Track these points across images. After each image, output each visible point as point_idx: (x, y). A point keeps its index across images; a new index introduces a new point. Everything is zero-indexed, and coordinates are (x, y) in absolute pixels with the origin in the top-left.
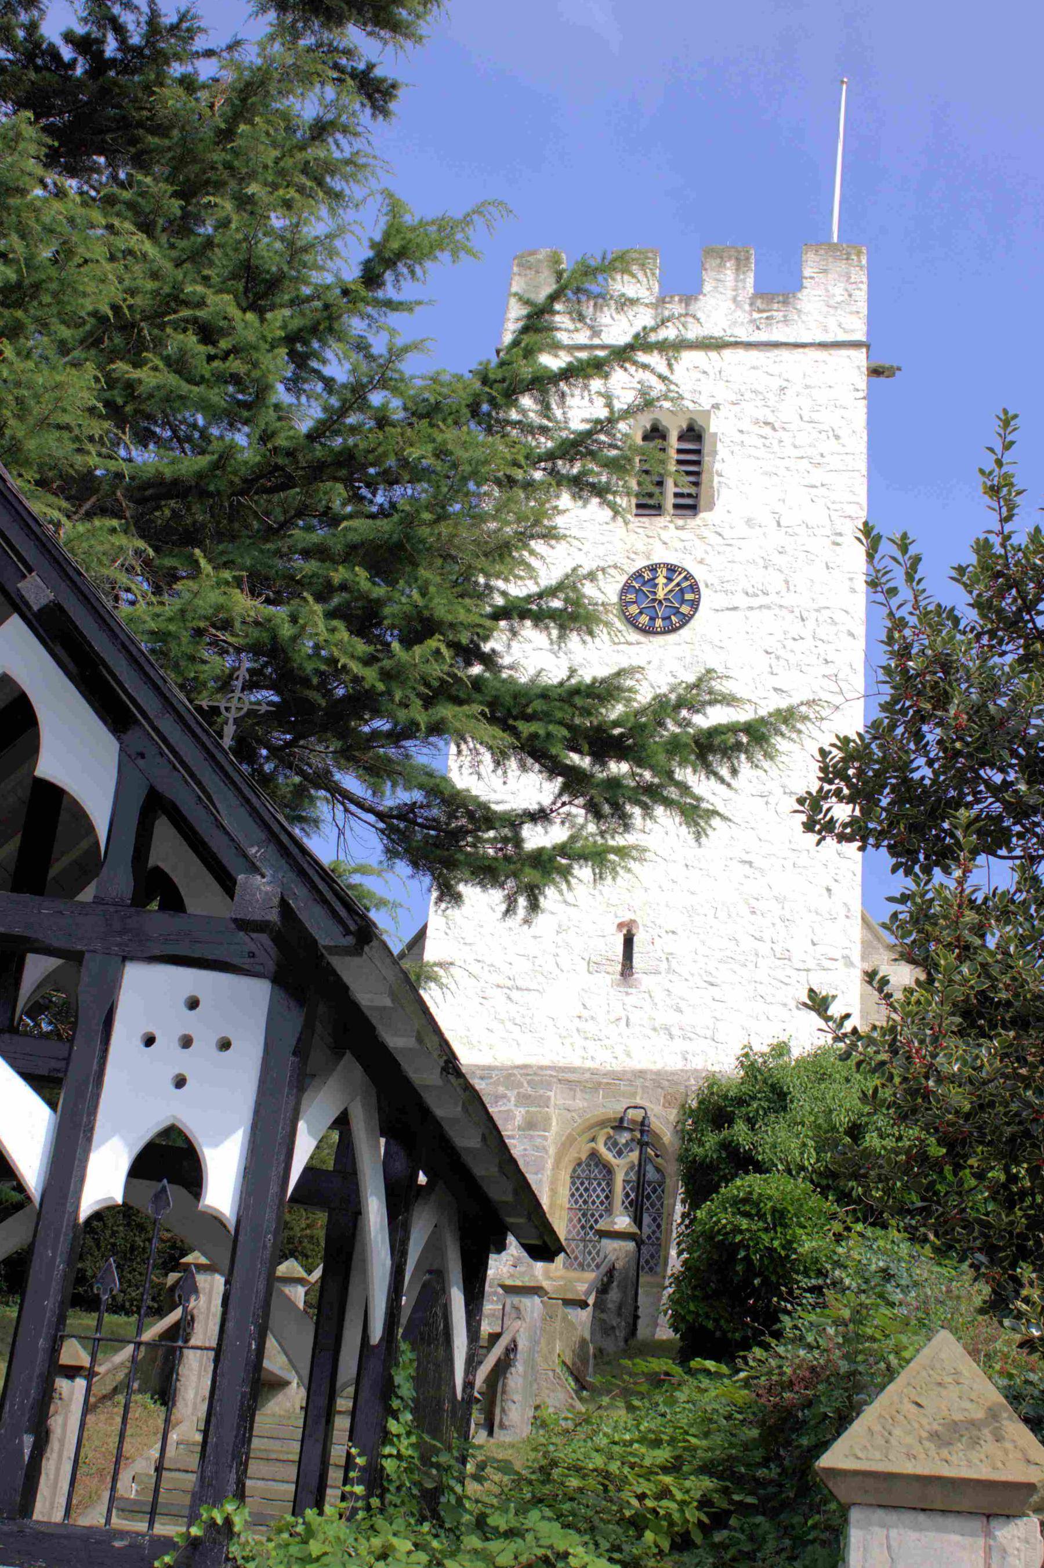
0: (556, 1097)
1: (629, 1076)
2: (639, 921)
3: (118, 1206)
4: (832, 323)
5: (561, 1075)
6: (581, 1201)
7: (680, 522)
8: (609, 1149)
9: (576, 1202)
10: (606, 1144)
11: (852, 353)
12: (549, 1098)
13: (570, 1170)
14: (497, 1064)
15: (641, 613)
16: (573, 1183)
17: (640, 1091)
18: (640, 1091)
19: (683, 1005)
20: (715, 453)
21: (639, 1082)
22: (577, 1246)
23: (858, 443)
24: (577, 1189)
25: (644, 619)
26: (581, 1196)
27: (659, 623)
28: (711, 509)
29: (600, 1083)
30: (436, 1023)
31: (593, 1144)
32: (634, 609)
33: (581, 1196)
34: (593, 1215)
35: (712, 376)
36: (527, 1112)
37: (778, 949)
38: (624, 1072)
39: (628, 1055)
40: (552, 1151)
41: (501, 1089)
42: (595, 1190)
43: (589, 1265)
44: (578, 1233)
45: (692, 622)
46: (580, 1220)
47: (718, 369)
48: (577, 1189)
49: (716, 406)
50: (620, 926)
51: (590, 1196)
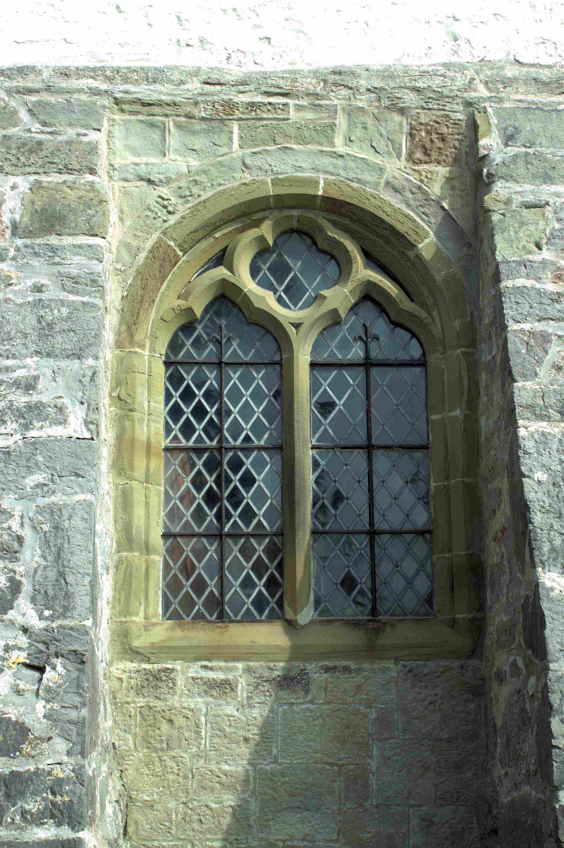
1: (309, 84)
5: (119, 89)
9: (187, 430)
10: (254, 271)
12: (93, 149)
13: (162, 347)
17: (342, 121)
18: (342, 121)
22: (200, 554)
24: (188, 395)
25: (128, 548)
26: (199, 412)
29: (230, 106)
31: (221, 272)
33: (199, 412)
34: (236, 465)
36: (37, 187)
38: (294, 75)
42: (236, 396)
43: (237, 605)
44: (199, 515)
46: (198, 482)
48: (188, 395)
51: (224, 413)
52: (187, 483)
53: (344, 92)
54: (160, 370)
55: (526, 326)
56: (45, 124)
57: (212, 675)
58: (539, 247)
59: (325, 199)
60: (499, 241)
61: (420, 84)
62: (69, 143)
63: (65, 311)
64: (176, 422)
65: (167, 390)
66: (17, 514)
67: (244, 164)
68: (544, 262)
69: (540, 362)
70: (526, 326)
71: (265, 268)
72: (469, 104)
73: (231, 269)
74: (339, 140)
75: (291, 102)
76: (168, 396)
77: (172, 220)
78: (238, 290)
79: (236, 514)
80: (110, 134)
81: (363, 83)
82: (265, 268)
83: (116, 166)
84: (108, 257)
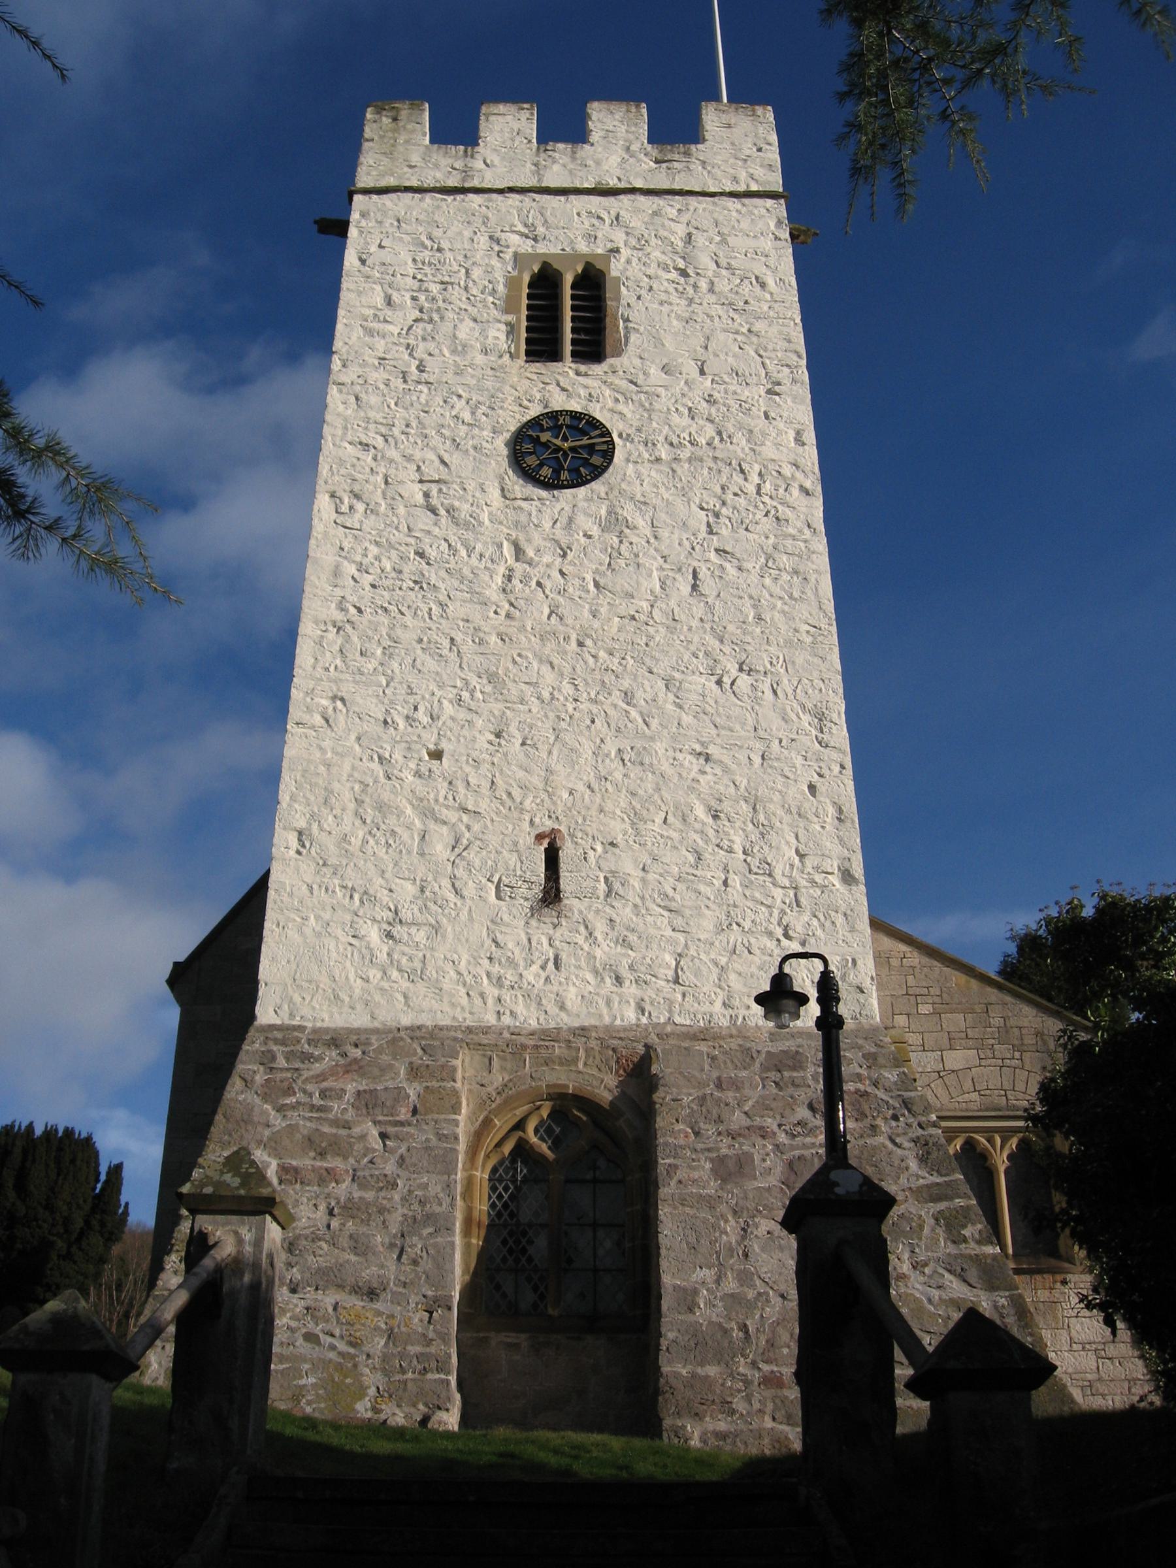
0: (464, 1065)
2: (563, 828)
3: (791, 1457)
4: (743, 175)
6: (506, 1215)
7: (583, 368)
8: (542, 1139)
11: (770, 203)
12: (454, 1069)
14: (376, 1024)
15: (541, 465)
16: (493, 1189)
19: (633, 938)
20: (618, 298)
21: (580, 1042)
23: (823, 561)
25: (546, 472)
27: (564, 475)
28: (618, 353)
30: (220, 924)
32: (532, 461)
35: (608, 221)
37: (754, 863)
39: (562, 1007)
40: (462, 1147)
41: (385, 1058)
44: (504, 1260)
45: (606, 475)
46: (504, 1242)
47: (613, 214)
49: (592, 145)
50: (539, 837)
52: (498, 1243)
53: (584, 1039)
54: (486, 1184)
55: (667, 1161)
56: (431, 1056)
57: (509, 1340)
58: (677, 1121)
59: (572, 1095)
60: (658, 1119)
61: (622, 1035)
62: (443, 1066)
63: (441, 1152)
64: (494, 1193)
65: (489, 1194)
66: (420, 1246)
67: (531, 1076)
68: (680, 1131)
69: (671, 1178)
70: (667, 1161)
71: (542, 1131)
72: (646, 1046)
73: (524, 1131)
74: (581, 1065)
75: (556, 1045)
76: (490, 1197)
77: (494, 1106)
78: (527, 1142)
79: (524, 1260)
80: (463, 1061)
81: (594, 1034)
82: (542, 1131)
83: (717, 289)
84: (462, 1124)
